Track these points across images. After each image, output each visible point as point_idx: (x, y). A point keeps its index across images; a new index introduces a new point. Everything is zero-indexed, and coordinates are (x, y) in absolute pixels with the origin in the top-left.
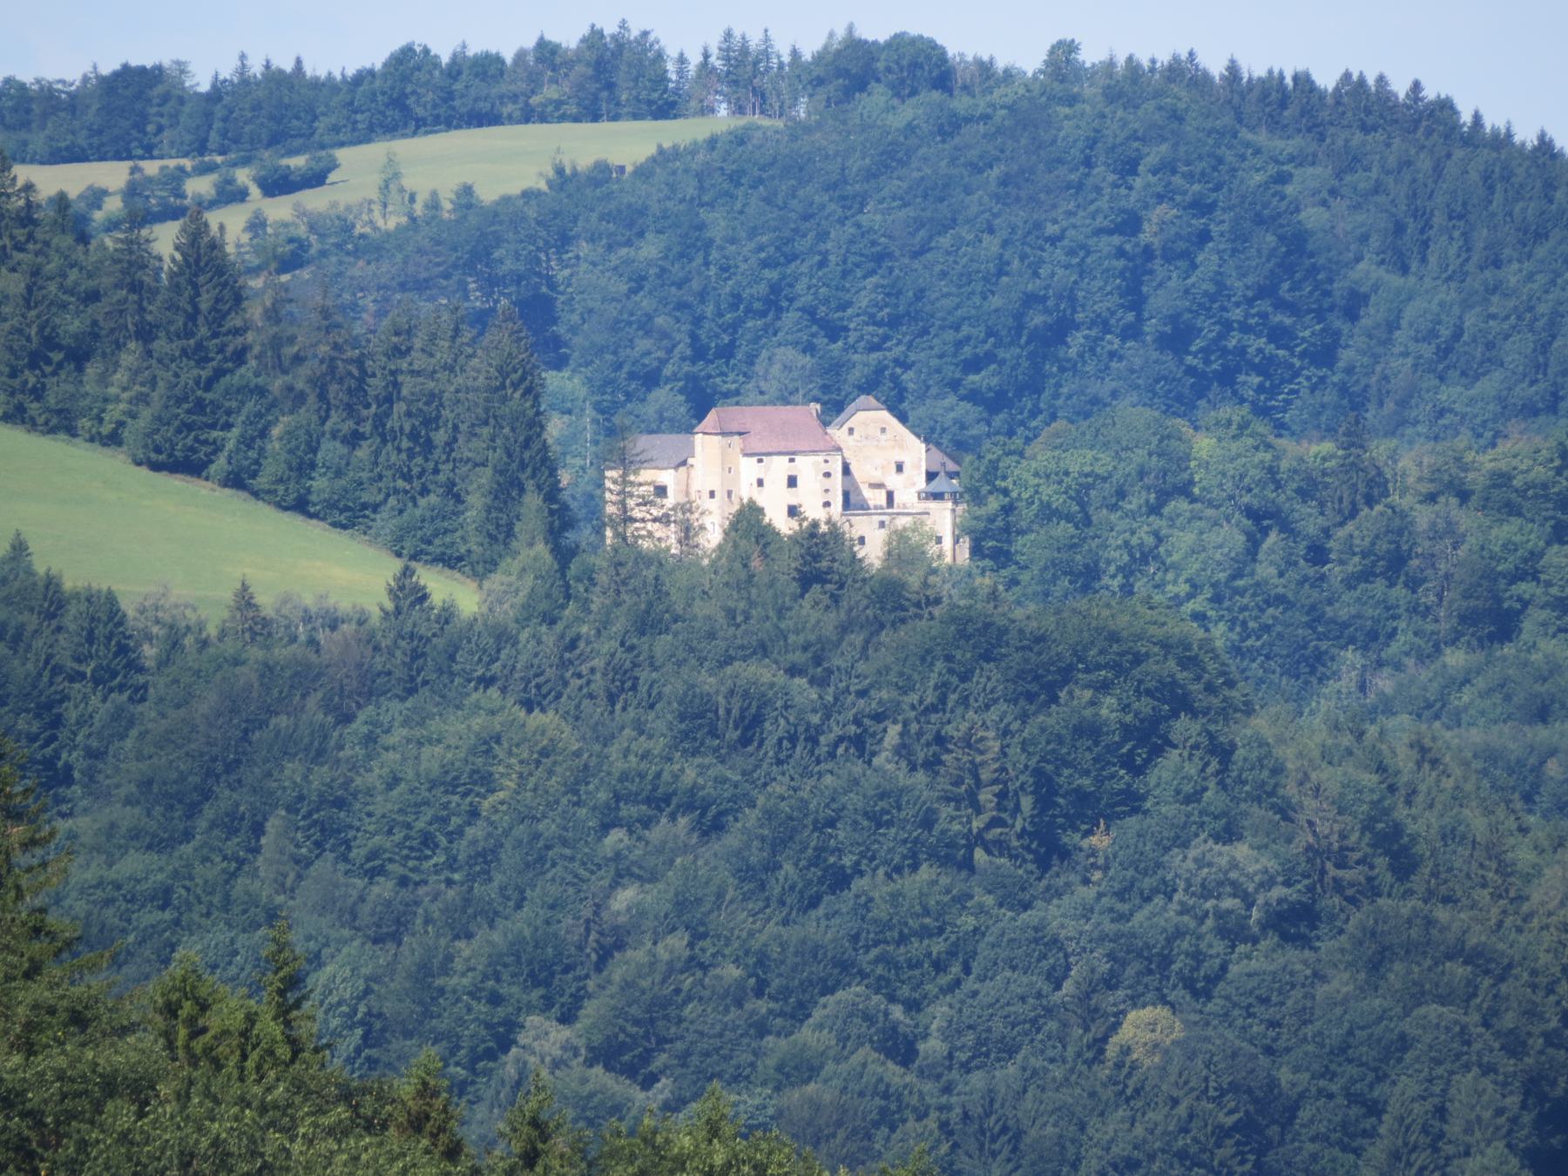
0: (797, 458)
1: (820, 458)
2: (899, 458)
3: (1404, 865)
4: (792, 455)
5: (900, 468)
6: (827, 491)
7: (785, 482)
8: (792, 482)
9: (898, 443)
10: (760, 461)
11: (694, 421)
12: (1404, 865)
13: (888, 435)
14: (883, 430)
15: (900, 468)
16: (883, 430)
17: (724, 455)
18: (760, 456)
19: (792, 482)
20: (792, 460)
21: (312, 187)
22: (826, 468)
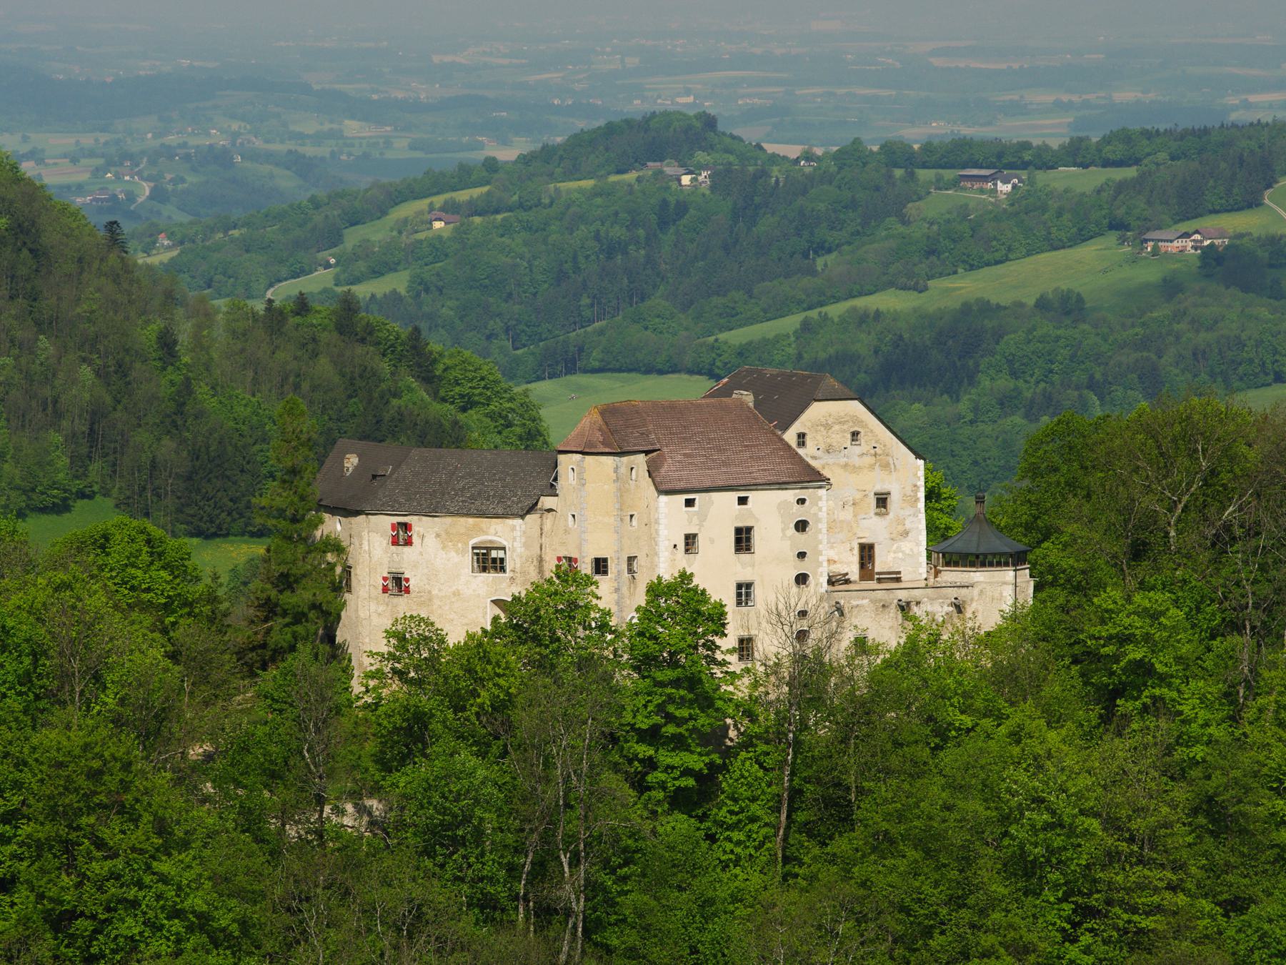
0: (752, 496)
1: (791, 495)
2: (879, 488)
3: (457, 878)
4: (742, 488)
5: (882, 501)
6: (802, 555)
7: (757, 537)
8: (743, 540)
9: (883, 462)
10: (690, 503)
11: (929, 485)
12: (457, 878)
13: (865, 445)
14: (855, 435)
15: (882, 501)
16: (855, 435)
17: (622, 494)
18: (689, 492)
19: (743, 540)
20: (743, 501)
21: (1117, 166)
22: (800, 513)
